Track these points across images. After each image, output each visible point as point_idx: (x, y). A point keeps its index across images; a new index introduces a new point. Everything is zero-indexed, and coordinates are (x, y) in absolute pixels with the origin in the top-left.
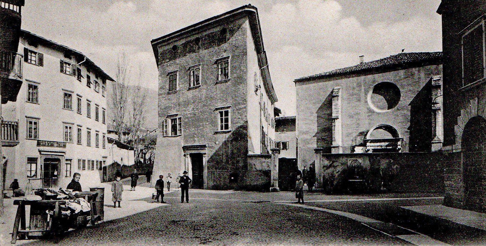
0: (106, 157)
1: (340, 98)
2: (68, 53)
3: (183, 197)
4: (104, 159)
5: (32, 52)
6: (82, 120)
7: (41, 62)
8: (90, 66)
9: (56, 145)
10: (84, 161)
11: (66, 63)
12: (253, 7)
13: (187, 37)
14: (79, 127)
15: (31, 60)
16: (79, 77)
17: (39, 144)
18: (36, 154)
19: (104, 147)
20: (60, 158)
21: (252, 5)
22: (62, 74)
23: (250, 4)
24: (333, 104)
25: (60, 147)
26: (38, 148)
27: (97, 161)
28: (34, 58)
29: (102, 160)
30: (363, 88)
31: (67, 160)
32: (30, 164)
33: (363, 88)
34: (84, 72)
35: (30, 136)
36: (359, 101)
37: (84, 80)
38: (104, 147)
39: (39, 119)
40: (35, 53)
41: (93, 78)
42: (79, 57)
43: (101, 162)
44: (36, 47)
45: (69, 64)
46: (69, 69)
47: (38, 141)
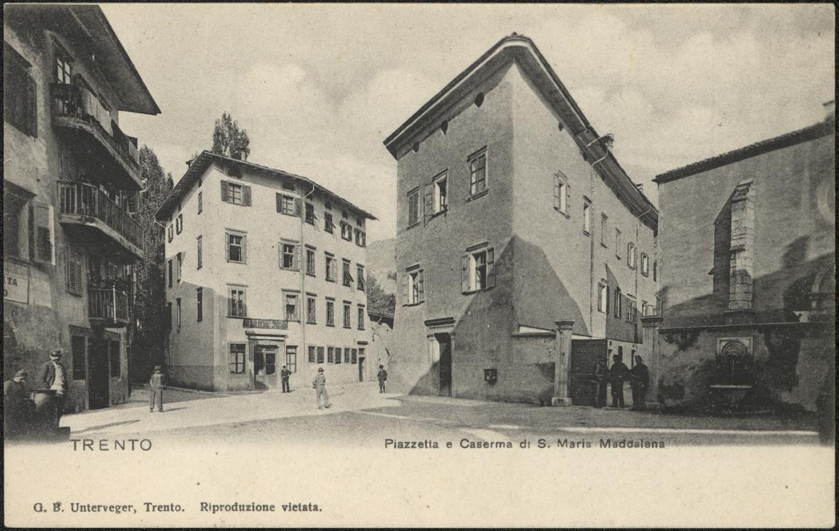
0: (365, 343)
1: (749, 204)
2: (288, 181)
3: (284, 387)
4: (362, 346)
5: (234, 185)
6: (318, 285)
7: (247, 201)
8: (330, 200)
9: (271, 325)
10: (339, 350)
11: (285, 197)
12: (522, 38)
13: (429, 125)
14: (311, 297)
15: (234, 198)
16: (310, 219)
17: (245, 325)
18: (243, 339)
19: (361, 328)
20: (278, 344)
21: (519, 33)
22: (280, 214)
23: (515, 34)
24: (733, 219)
25: (278, 328)
26: (246, 329)
27: (347, 350)
28: (239, 194)
29: (357, 347)
30: (807, 174)
31: (288, 347)
32: (235, 354)
33: (807, 174)
34: (319, 210)
35: (234, 313)
36: (796, 204)
37: (321, 222)
38: (361, 328)
39: (315, 295)
40: (239, 187)
41: (337, 217)
42: (305, 185)
43: (354, 350)
44: (239, 177)
45: (291, 198)
46: (292, 206)
47: (245, 319)
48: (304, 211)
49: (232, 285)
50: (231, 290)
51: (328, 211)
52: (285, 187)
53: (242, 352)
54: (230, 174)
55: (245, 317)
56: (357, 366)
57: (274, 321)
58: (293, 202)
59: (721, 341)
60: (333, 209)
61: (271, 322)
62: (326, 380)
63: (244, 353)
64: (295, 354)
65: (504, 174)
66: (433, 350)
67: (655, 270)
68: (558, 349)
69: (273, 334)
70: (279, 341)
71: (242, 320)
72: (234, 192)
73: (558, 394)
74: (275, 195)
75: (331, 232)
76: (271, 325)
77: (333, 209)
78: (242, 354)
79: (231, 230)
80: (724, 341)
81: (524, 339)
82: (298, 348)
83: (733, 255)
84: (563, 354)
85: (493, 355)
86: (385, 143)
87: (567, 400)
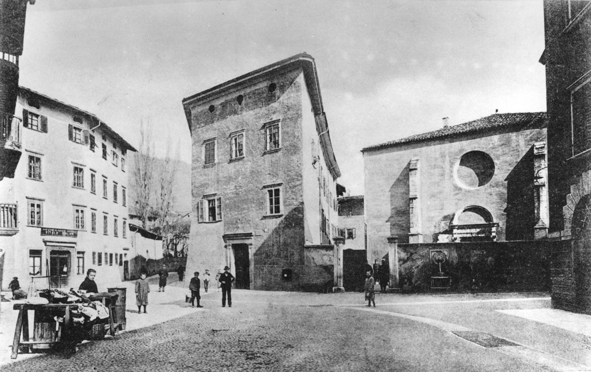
2: (79, 115)
5: (32, 114)
7: (44, 129)
27: (116, 255)
28: (37, 122)
29: (123, 252)
31: (79, 253)
37: (99, 150)
40: (37, 116)
42: (93, 121)
44: (38, 108)
45: (80, 130)
46: (80, 136)
48: (89, 141)
49: (31, 199)
50: (30, 203)
51: (104, 142)
52: (75, 120)
53: (38, 257)
54: (31, 104)
55: (42, 227)
56: (122, 267)
57: (66, 230)
58: (81, 133)
59: (432, 252)
60: (107, 140)
61: (65, 231)
62: (315, 257)
63: (41, 257)
64: (83, 258)
65: (192, 108)
66: (230, 257)
67: (124, 195)
68: (335, 256)
69: (52, 240)
70: (71, 247)
71: (40, 229)
72: (32, 119)
73: (337, 285)
74: (68, 125)
75: (106, 159)
76: (64, 233)
77: (107, 140)
78: (39, 258)
79: (36, 153)
80: (434, 251)
81: (312, 250)
82: (85, 254)
83: (411, 201)
84: (339, 259)
85: (287, 260)
86: (184, 100)
87: (342, 288)
